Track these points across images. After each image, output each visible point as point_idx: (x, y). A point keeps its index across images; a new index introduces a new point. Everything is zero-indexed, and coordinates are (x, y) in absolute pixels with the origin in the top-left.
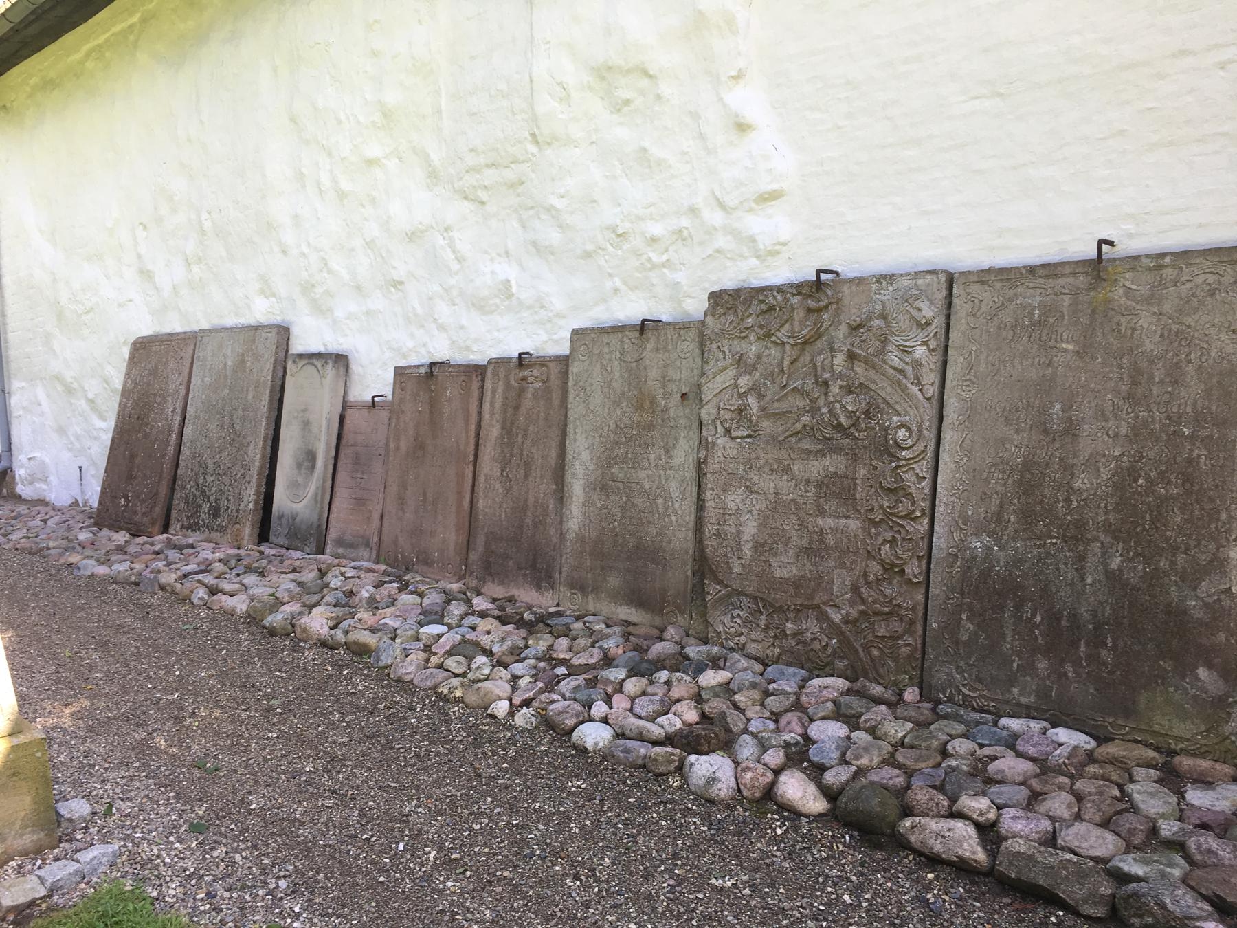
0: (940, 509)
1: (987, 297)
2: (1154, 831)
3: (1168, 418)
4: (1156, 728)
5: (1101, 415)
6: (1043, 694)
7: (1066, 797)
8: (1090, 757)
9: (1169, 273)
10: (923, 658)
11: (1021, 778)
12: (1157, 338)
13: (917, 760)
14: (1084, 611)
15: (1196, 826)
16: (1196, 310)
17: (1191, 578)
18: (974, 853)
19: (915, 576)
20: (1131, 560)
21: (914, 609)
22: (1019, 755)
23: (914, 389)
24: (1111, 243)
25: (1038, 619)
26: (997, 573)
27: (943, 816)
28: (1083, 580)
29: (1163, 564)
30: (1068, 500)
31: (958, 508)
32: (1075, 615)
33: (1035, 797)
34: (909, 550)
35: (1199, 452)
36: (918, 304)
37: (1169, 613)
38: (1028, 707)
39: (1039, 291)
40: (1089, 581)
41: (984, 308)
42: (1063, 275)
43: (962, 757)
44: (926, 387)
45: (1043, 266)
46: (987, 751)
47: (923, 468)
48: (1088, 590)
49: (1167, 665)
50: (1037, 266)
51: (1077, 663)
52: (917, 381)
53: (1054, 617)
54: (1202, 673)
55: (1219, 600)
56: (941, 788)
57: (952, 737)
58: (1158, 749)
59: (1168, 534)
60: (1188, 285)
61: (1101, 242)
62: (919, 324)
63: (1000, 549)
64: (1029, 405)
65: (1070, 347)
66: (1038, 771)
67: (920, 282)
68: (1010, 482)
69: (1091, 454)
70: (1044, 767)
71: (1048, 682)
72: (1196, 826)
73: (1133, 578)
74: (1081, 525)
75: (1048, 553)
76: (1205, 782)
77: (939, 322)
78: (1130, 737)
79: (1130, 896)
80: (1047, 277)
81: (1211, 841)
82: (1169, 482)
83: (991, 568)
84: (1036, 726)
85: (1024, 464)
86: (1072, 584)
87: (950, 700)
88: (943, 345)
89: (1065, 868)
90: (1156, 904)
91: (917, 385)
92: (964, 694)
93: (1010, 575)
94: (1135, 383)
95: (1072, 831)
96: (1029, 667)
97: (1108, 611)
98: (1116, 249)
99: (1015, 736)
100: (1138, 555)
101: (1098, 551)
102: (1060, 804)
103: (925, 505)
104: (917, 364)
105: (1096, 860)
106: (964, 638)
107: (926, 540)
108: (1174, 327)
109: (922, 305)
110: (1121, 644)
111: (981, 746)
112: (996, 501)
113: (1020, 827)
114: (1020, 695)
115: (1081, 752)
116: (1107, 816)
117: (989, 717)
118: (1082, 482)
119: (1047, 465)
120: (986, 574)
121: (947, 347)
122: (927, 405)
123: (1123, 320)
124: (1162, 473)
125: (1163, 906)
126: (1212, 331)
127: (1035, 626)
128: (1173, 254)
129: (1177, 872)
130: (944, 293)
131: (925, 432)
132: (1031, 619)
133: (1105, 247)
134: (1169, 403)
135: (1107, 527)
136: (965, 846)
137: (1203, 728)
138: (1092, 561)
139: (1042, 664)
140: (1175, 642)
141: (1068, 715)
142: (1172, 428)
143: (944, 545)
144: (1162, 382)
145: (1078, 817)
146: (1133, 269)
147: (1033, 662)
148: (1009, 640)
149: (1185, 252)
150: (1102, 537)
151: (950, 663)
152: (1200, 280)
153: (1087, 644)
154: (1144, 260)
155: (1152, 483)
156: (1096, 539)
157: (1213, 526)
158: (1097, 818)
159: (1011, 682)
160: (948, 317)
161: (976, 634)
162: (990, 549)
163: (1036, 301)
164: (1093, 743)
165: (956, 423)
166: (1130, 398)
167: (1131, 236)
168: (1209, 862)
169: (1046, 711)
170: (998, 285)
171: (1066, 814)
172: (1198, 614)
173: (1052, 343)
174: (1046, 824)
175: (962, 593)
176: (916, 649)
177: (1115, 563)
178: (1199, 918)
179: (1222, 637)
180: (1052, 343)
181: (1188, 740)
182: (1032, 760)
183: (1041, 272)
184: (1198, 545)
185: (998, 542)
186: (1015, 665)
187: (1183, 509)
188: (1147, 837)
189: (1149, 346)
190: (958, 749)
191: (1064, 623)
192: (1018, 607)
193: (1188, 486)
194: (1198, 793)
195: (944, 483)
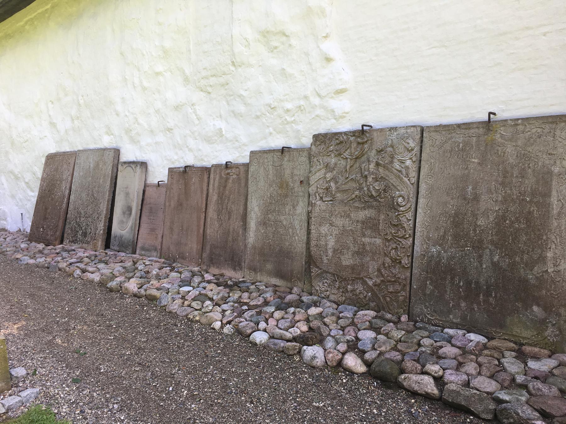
0: (418, 234)
2: (513, 380)
3: (520, 193)
4: (514, 333)
5: (489, 191)
6: (464, 318)
7: (474, 365)
8: (485, 347)
9: (520, 128)
10: (410, 302)
12: (515, 157)
13: (407, 348)
14: (482, 280)
15: (532, 378)
16: (532, 144)
17: (530, 265)
19: (406, 264)
21: (405, 279)
22: (453, 345)
23: (406, 179)
24: (494, 114)
25: (461, 284)
26: (443, 263)
27: (419, 374)
28: (481, 266)
30: (475, 230)
31: (425, 234)
32: (478, 282)
33: (460, 365)
35: (534, 208)
38: (457, 324)
39: (462, 135)
40: (484, 266)
42: (473, 128)
45: (464, 124)
46: (439, 344)
47: (410, 215)
48: (484, 271)
49: (519, 305)
51: (479, 304)
52: (407, 175)
53: (468, 283)
54: (535, 308)
55: (543, 275)
56: (418, 361)
57: (423, 337)
58: (515, 343)
59: (520, 245)
60: (529, 133)
61: (490, 113)
62: (408, 150)
63: (444, 252)
65: (476, 161)
66: (461, 353)
67: (408, 131)
68: (449, 222)
69: (485, 209)
71: (466, 313)
73: (504, 264)
74: (481, 241)
75: (466, 254)
76: (536, 358)
77: (417, 149)
78: (503, 337)
79: (503, 410)
80: (466, 129)
81: (539, 385)
82: (520, 222)
84: (460, 332)
86: (477, 268)
87: (422, 321)
89: (474, 397)
90: (515, 413)
91: (407, 178)
93: (449, 263)
94: (505, 177)
95: (476, 380)
97: (493, 280)
98: (496, 116)
99: (451, 337)
100: (506, 255)
101: (488, 253)
102: (471, 368)
104: (407, 168)
105: (488, 393)
107: (411, 248)
108: (523, 152)
109: (409, 141)
110: (498, 295)
111: (436, 341)
112: (442, 230)
113: (453, 378)
117: (440, 328)
118: (481, 222)
119: (466, 214)
120: (438, 263)
122: (412, 187)
123: (499, 148)
125: (518, 414)
126: (540, 154)
128: (522, 119)
129: (524, 399)
130: (419, 135)
131: (411, 199)
135: (492, 242)
137: (535, 333)
138: (486, 258)
139: (463, 304)
140: (523, 294)
141: (475, 327)
142: (521, 197)
143: (419, 250)
144: (517, 177)
145: (479, 374)
146: (504, 126)
148: (448, 293)
149: (528, 118)
150: (490, 246)
151: (422, 304)
153: (483, 296)
154: (509, 122)
157: (540, 242)
158: (488, 374)
159: (449, 312)
160: (421, 147)
161: (433, 290)
162: (440, 252)
163: (461, 140)
165: (425, 195)
166: (503, 184)
167: (503, 111)
168: (538, 394)
169: (465, 326)
170: (444, 132)
172: (533, 282)
173: (468, 159)
174: (465, 377)
175: (427, 272)
177: (496, 258)
178: (534, 419)
179: (544, 292)
180: (468, 159)
181: (529, 339)
183: (463, 127)
185: (443, 249)
186: (451, 305)
187: (526, 234)
189: (511, 160)
190: (425, 343)
191: (473, 286)
192: (452, 278)
194: (533, 363)
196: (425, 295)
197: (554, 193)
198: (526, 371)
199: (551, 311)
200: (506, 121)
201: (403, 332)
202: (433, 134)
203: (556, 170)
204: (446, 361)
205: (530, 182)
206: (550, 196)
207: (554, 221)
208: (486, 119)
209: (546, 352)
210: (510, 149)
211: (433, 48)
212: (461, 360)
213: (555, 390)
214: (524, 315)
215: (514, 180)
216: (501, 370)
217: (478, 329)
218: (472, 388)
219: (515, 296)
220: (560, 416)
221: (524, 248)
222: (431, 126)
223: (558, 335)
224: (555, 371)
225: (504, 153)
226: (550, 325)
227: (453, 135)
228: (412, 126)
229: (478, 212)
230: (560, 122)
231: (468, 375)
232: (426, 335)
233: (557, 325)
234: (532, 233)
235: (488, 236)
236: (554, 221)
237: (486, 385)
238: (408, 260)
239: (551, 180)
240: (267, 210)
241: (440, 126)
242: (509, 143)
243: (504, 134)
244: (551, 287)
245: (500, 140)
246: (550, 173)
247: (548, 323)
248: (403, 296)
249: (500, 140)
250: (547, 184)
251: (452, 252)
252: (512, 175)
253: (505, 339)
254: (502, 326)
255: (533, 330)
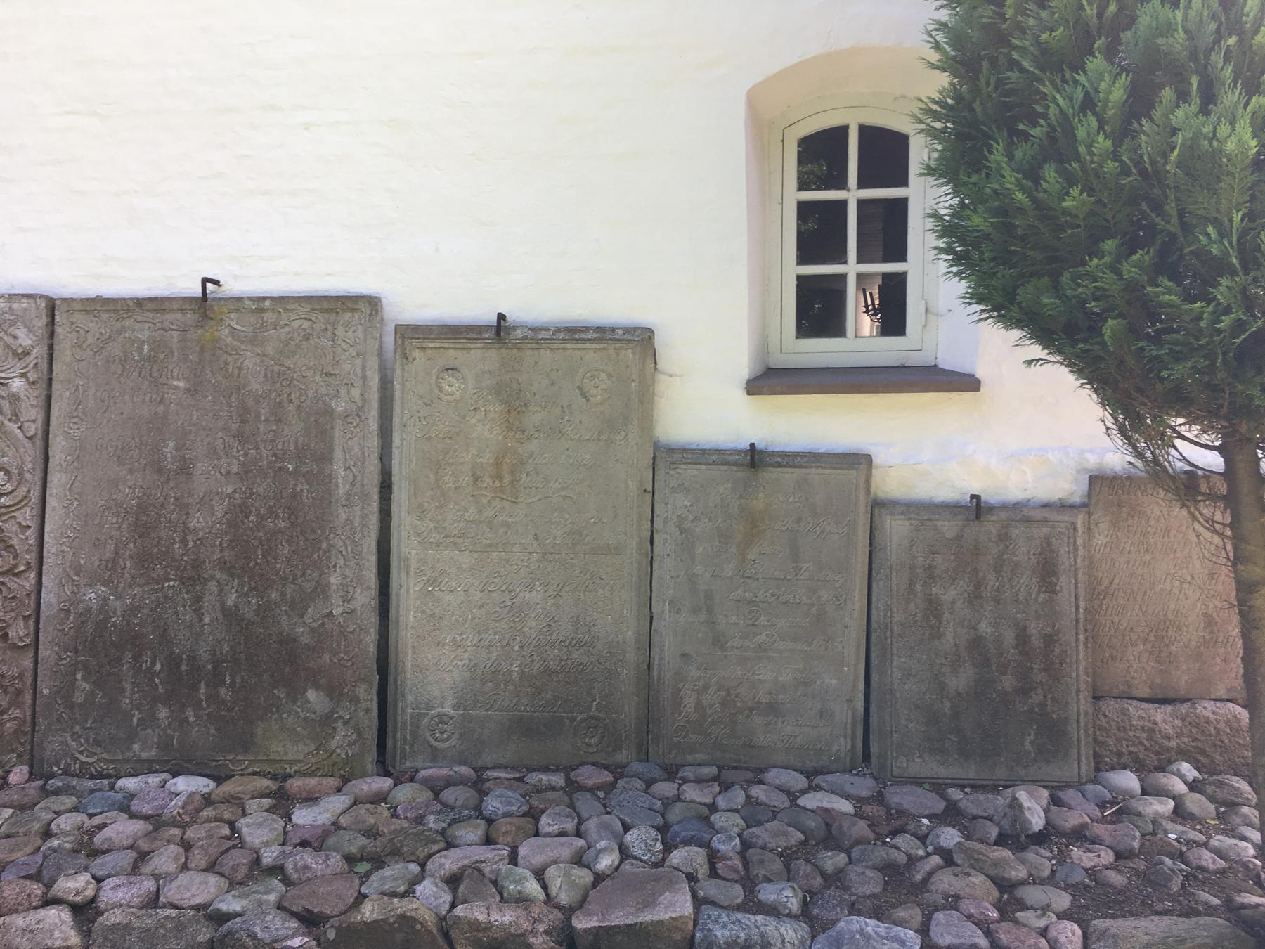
0: (49, 560)
1: (94, 328)
2: (257, 860)
3: (275, 455)
4: (273, 756)
5: (213, 452)
6: (164, 745)
7: (174, 849)
8: (208, 800)
9: (269, 317)
10: (34, 730)
11: (130, 841)
12: (261, 378)
13: (12, 851)
14: (203, 653)
15: (296, 845)
16: (294, 353)
17: (298, 607)
18: (66, 939)
19: (21, 639)
20: (246, 595)
21: (21, 676)
22: (133, 816)
23: (13, 427)
24: (217, 283)
25: (158, 667)
26: (114, 625)
27: (36, 908)
28: (201, 620)
29: (274, 596)
30: (184, 541)
31: (69, 557)
32: (194, 657)
33: (143, 856)
34: (12, 610)
35: (302, 486)
36: (13, 330)
37: (281, 642)
38: (150, 762)
39: (147, 325)
40: (207, 620)
41: (90, 340)
42: (172, 311)
43: (65, 834)
44: (26, 424)
45: (150, 299)
46: (96, 821)
47: (27, 515)
48: (207, 629)
49: (280, 693)
50: (144, 299)
51: (197, 706)
52: (15, 417)
53: (173, 663)
54: (311, 695)
55: (323, 624)
56: (35, 877)
57: (58, 813)
58: (274, 777)
59: (278, 566)
60: (287, 329)
61: (205, 281)
62: (15, 353)
63: (117, 598)
64: (142, 444)
65: (181, 384)
66: (151, 828)
67: (15, 306)
68: (125, 526)
69: (205, 493)
70: (157, 822)
71: (169, 731)
72: (296, 845)
73: (247, 612)
74: (197, 565)
75: (166, 597)
76: (311, 799)
77: (39, 352)
78: (249, 771)
79: (225, 936)
80: (156, 311)
81: (307, 857)
82: (277, 517)
83: (106, 620)
84: (154, 780)
85: (139, 506)
86: (191, 626)
87: (66, 772)
88: (45, 378)
89: (163, 926)
90: (249, 936)
91: (15, 422)
92: (82, 763)
93: (128, 624)
94: (243, 421)
95: (175, 885)
96: (149, 720)
97: (226, 648)
98: (222, 289)
99: (131, 796)
100: (252, 589)
101: (215, 590)
102: (166, 859)
103: (31, 557)
104: (14, 398)
105: (197, 908)
106: (80, 701)
107: (33, 597)
108: (276, 368)
109: (17, 332)
110: (238, 679)
111: (91, 816)
112: (110, 547)
113: (120, 895)
114: (142, 750)
115: (198, 797)
116: (213, 858)
117: (105, 782)
118: (197, 521)
119: (162, 505)
120: (102, 626)
121: (50, 380)
122: (28, 444)
123: (230, 359)
124: (271, 507)
125: (253, 936)
126: (309, 374)
127: (155, 675)
128: (272, 298)
129: (272, 898)
130: (45, 320)
131: (27, 475)
132: (151, 668)
133: (209, 286)
134: (274, 441)
135: (222, 564)
136: (57, 934)
137: (313, 747)
138: (210, 601)
139: (163, 714)
140: (287, 670)
141: (190, 761)
142: (278, 464)
143: (54, 601)
144: (267, 420)
145: (185, 867)
146: (237, 310)
147: (154, 714)
148: (128, 693)
149: (282, 298)
150: (218, 575)
151: (64, 730)
152: (296, 324)
153: (207, 685)
154: (247, 302)
155: (262, 518)
156: (212, 577)
157: (316, 556)
158: (203, 864)
159: (131, 738)
160: (51, 347)
161: (92, 693)
162: (106, 599)
163: (144, 336)
164: (212, 784)
165: (64, 464)
166: (240, 436)
167: (236, 277)
168: (304, 878)
169: (168, 762)
170: (105, 316)
171: (172, 868)
172: (305, 640)
173: (163, 380)
174: (150, 885)
175: (76, 651)
176: (24, 721)
177: (231, 600)
178: (287, 938)
179: (326, 657)
180: (163, 380)
181: (301, 761)
182: (146, 818)
183: (149, 305)
184: (303, 574)
185: (114, 590)
186: (135, 720)
187: (290, 542)
188: (251, 869)
189: (254, 386)
190: (63, 826)
191: (184, 667)
192: (137, 658)
193: (293, 518)
194: (304, 812)
195: (52, 530)
196: (71, 706)
197: (338, 454)
198: (285, 833)
199: (341, 694)
200: (240, 299)
201: (10, 811)
202: (78, 317)
203: (340, 406)
204: (108, 858)
205: (293, 431)
206: (331, 460)
207: (341, 510)
208: (199, 293)
209: (332, 782)
210: (250, 361)
211: (67, 113)
212: (144, 845)
213: (336, 861)
214: (289, 713)
215: (262, 428)
216: (234, 847)
217: (197, 764)
218: (164, 906)
219: (272, 676)
220: (341, 914)
221: (287, 571)
222: (73, 300)
223: (355, 743)
224: (343, 821)
225: (240, 369)
226: (339, 724)
227: (127, 323)
228: (24, 296)
229: (191, 500)
230: (344, 310)
231: (156, 877)
232: (69, 806)
233: (352, 722)
234: (301, 538)
235: (213, 552)
236: (341, 510)
237: (197, 888)
238: (26, 627)
239: (332, 428)
240: (1238, 241)
241: (98, 300)
242: (249, 347)
243: (238, 327)
244: (339, 644)
245: (229, 340)
246: (329, 412)
247: (336, 721)
248: (15, 719)
249: (229, 340)
250: (324, 434)
251: (134, 597)
252: (258, 416)
253: (254, 774)
254: (246, 744)
255: (308, 742)
